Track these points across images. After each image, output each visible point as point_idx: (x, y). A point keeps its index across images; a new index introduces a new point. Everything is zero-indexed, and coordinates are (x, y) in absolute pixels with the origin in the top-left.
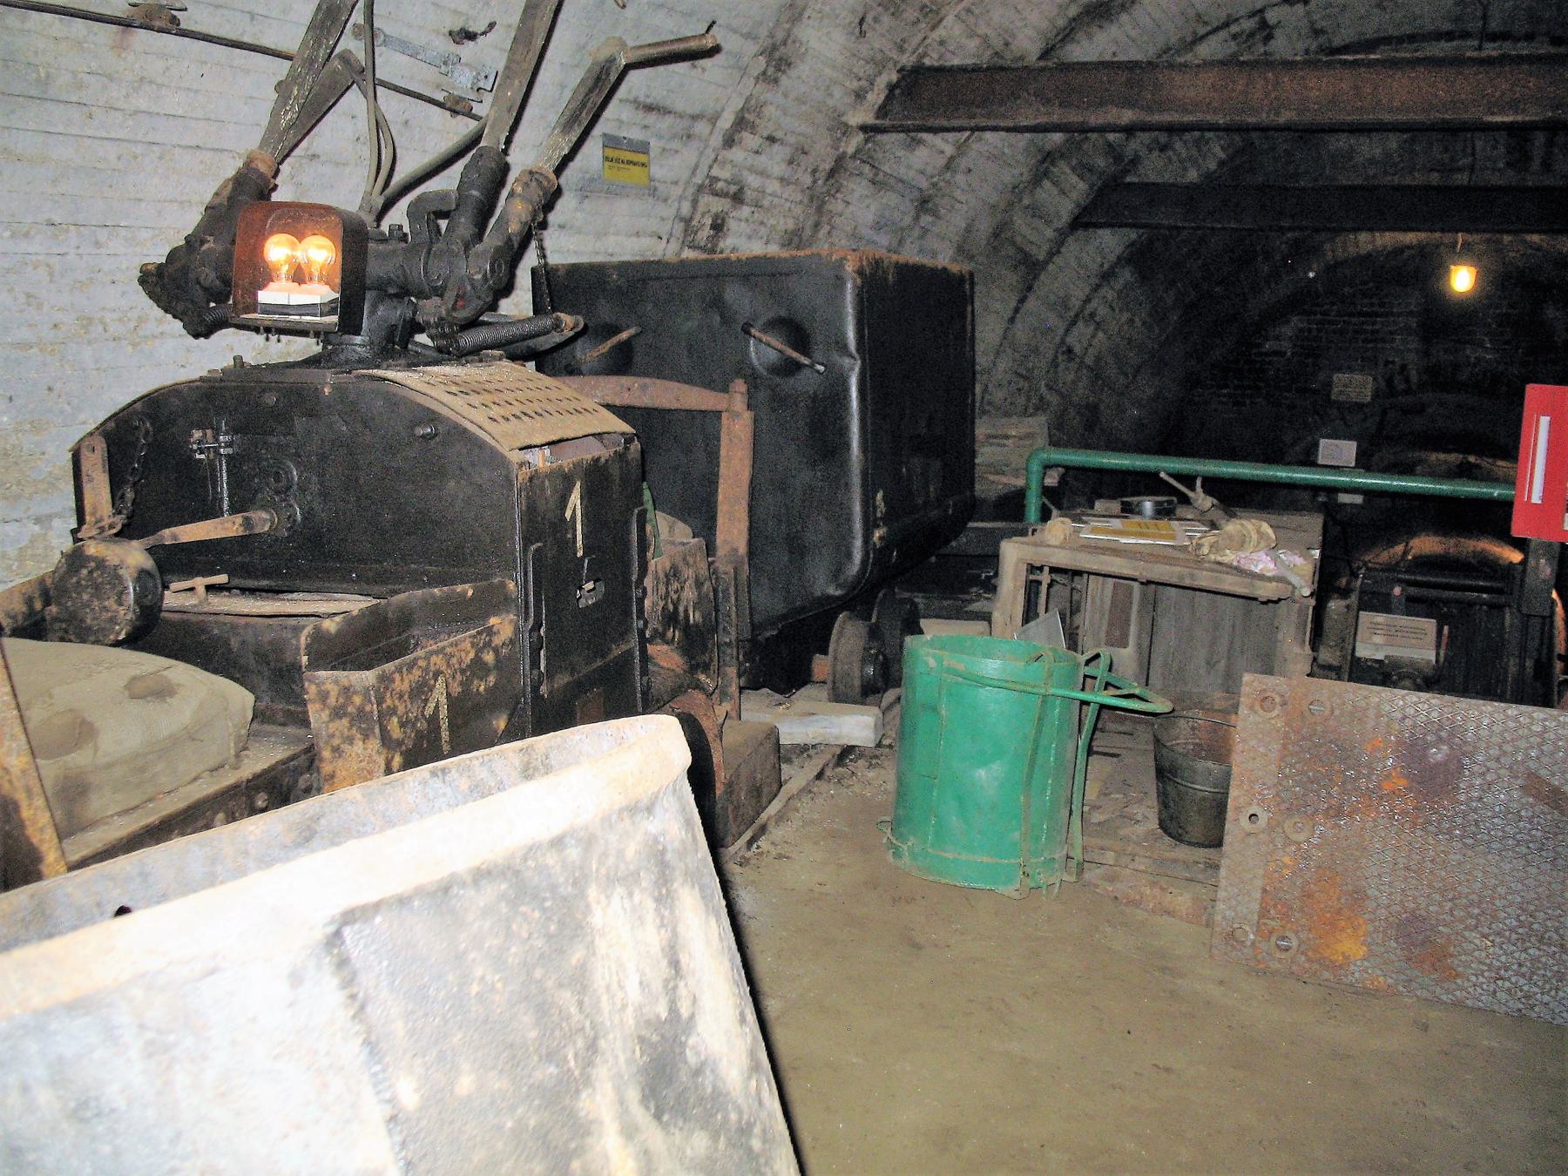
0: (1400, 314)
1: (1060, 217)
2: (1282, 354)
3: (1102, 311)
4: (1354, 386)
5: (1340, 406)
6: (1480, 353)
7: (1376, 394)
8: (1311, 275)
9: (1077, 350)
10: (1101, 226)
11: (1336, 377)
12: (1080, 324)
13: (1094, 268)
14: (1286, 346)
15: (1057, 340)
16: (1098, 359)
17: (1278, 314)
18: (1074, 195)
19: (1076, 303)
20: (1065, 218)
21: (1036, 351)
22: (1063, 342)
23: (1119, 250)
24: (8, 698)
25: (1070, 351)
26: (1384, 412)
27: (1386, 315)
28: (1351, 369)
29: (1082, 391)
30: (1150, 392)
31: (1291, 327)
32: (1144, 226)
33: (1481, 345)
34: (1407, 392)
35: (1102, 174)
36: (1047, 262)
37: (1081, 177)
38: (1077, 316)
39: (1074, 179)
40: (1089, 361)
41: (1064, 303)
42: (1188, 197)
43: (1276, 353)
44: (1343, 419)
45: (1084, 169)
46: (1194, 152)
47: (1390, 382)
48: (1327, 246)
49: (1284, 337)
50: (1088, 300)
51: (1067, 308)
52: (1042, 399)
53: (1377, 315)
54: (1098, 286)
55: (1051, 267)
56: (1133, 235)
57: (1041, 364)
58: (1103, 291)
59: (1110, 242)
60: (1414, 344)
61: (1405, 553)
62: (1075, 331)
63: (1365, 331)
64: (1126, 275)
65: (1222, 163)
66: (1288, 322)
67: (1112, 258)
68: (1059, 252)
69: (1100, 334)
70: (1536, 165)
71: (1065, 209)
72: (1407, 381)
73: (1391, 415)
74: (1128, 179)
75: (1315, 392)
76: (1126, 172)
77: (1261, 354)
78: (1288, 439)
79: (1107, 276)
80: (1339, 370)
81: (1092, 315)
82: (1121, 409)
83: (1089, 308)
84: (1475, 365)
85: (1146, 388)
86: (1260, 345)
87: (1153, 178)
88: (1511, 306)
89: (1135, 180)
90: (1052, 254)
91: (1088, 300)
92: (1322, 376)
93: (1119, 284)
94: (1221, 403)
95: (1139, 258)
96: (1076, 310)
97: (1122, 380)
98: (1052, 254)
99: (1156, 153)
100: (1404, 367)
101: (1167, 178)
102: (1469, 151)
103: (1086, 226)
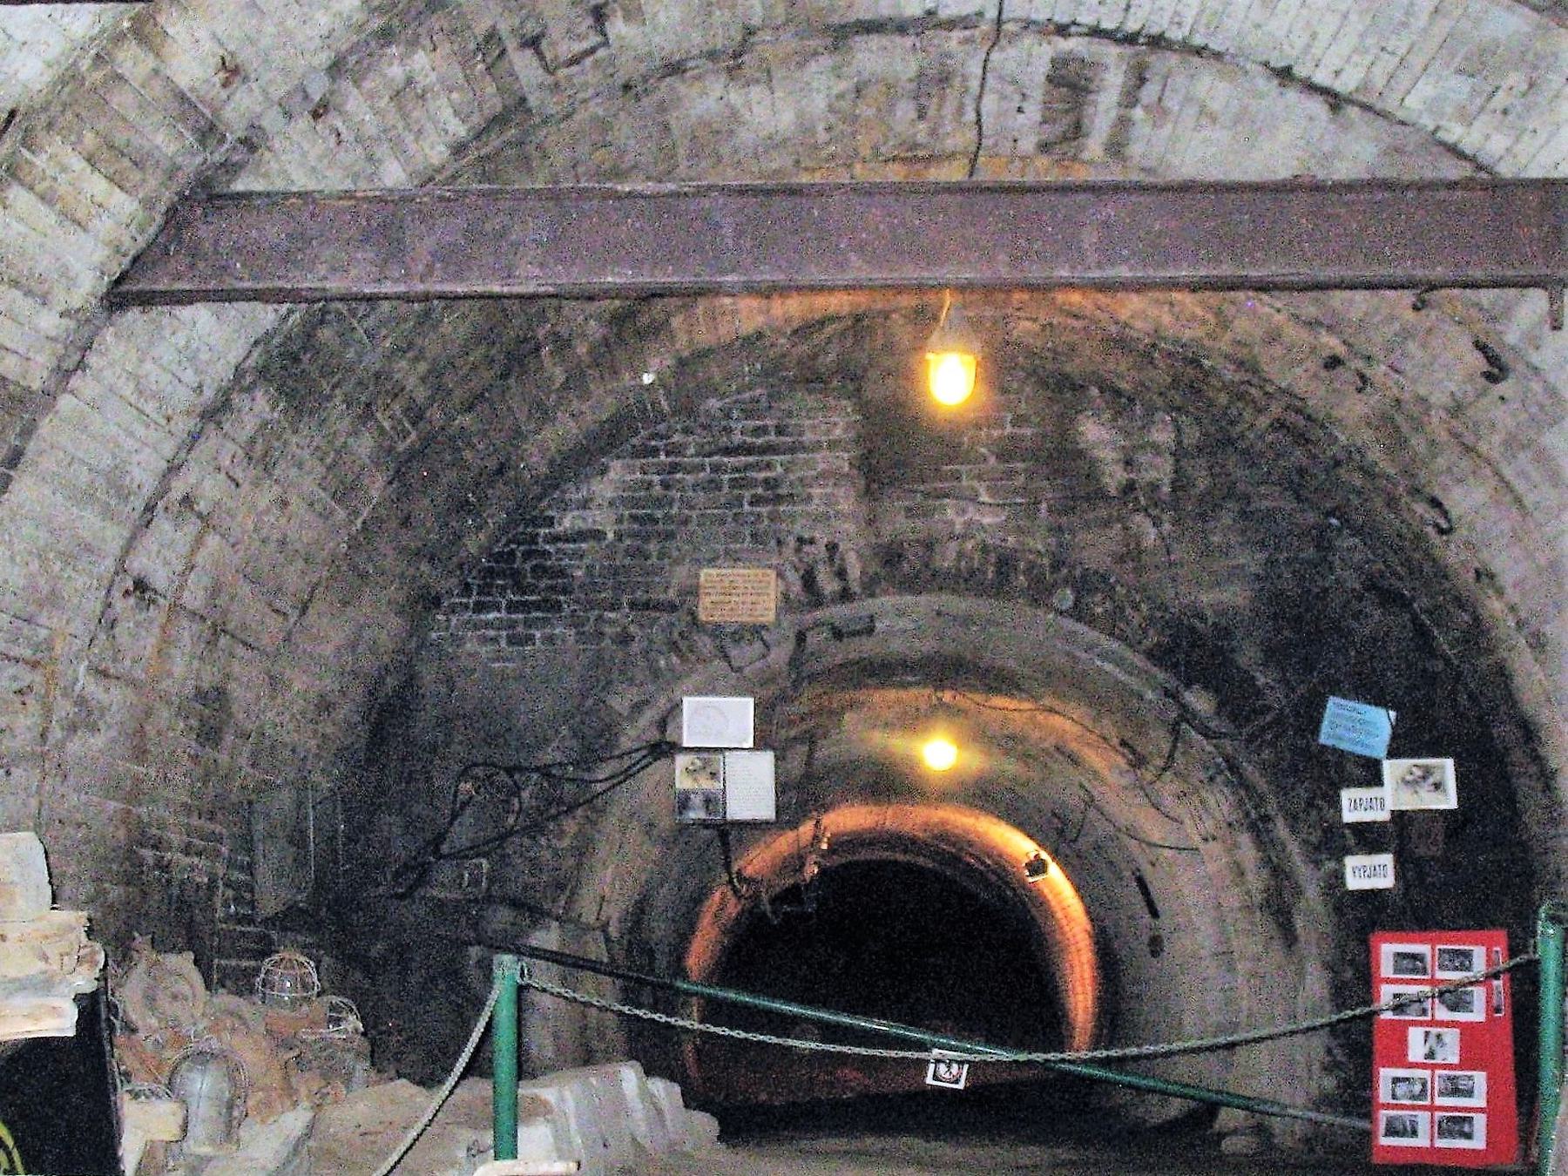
0: (817, 446)
1: (72, 283)
2: (598, 535)
3: (211, 490)
4: (742, 591)
5: (717, 631)
6: (972, 513)
7: (787, 603)
8: (647, 379)
9: (160, 579)
10: (187, 298)
11: (707, 574)
12: (163, 525)
13: (182, 397)
14: (602, 519)
15: (109, 564)
16: (215, 591)
17: (582, 459)
18: (104, 226)
19: (144, 474)
20: (87, 286)
21: (53, 599)
22: (121, 568)
23: (235, 355)
24: (885, 9)
25: (141, 585)
26: (801, 638)
27: (792, 450)
28: (735, 558)
29: (184, 669)
30: (338, 637)
31: (615, 478)
32: (278, 296)
33: (974, 499)
34: (845, 595)
35: (173, 172)
36: (50, 396)
37: (117, 181)
38: (150, 508)
39: (97, 186)
40: (194, 597)
41: (116, 483)
42: (382, 221)
43: (581, 536)
44: (726, 657)
45: (114, 159)
46: (393, 118)
47: (809, 580)
48: (676, 322)
49: (600, 502)
50: (173, 469)
51: (124, 495)
52: (81, 701)
53: (770, 449)
54: (195, 437)
55: (65, 403)
56: (266, 316)
57: (68, 628)
58: (207, 447)
59: (210, 338)
60: (847, 500)
61: (816, 838)
62: (150, 542)
63: (753, 483)
64: (258, 407)
65: (459, 149)
66: (604, 471)
67: (222, 372)
68: (81, 365)
69: (213, 541)
70: (1094, 146)
71: (85, 264)
72: (841, 574)
73: (813, 640)
74: (239, 186)
75: (673, 608)
76: (230, 168)
77: (556, 539)
78: (619, 703)
79: (215, 413)
80: (712, 562)
81: (187, 501)
82: (275, 683)
83: (178, 488)
84: (964, 537)
85: (330, 632)
86: (550, 522)
87: (302, 181)
88: (1019, 421)
89: (259, 186)
90: (63, 375)
91: (173, 469)
92: (680, 574)
93: (247, 425)
94: (485, 640)
95: (291, 370)
96: (147, 491)
97: (274, 622)
98: (63, 375)
99: (303, 122)
100: (832, 548)
101: (335, 181)
102: (971, 116)
103: (147, 300)
